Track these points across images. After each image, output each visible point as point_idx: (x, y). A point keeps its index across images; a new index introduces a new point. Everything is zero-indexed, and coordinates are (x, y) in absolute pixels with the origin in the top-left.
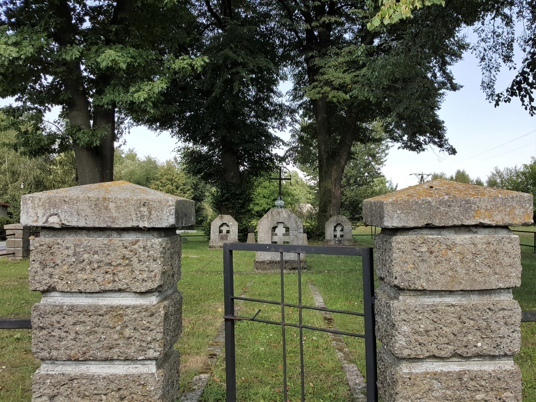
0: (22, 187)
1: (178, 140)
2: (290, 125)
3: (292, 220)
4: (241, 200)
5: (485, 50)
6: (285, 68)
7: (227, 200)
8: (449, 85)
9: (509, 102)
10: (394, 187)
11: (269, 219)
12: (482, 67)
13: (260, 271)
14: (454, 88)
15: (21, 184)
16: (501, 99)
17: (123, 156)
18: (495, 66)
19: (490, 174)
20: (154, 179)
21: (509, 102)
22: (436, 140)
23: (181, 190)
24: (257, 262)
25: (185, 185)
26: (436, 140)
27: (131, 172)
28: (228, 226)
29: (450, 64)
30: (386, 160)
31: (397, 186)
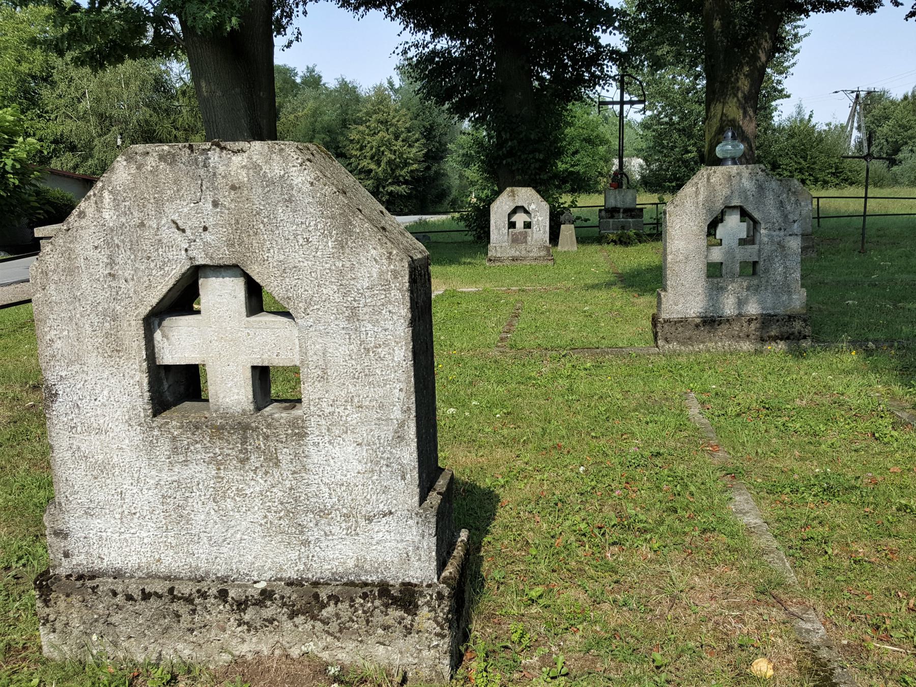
0: (119, 142)
1: (402, 26)
3: (770, 201)
4: (540, 152)
7: (510, 153)
10: (807, 117)
15: (116, 138)
17: (298, 80)
20: (355, 123)
23: (403, 141)
25: (409, 132)
27: (315, 111)
28: (527, 212)
30: (794, 64)
31: (811, 116)
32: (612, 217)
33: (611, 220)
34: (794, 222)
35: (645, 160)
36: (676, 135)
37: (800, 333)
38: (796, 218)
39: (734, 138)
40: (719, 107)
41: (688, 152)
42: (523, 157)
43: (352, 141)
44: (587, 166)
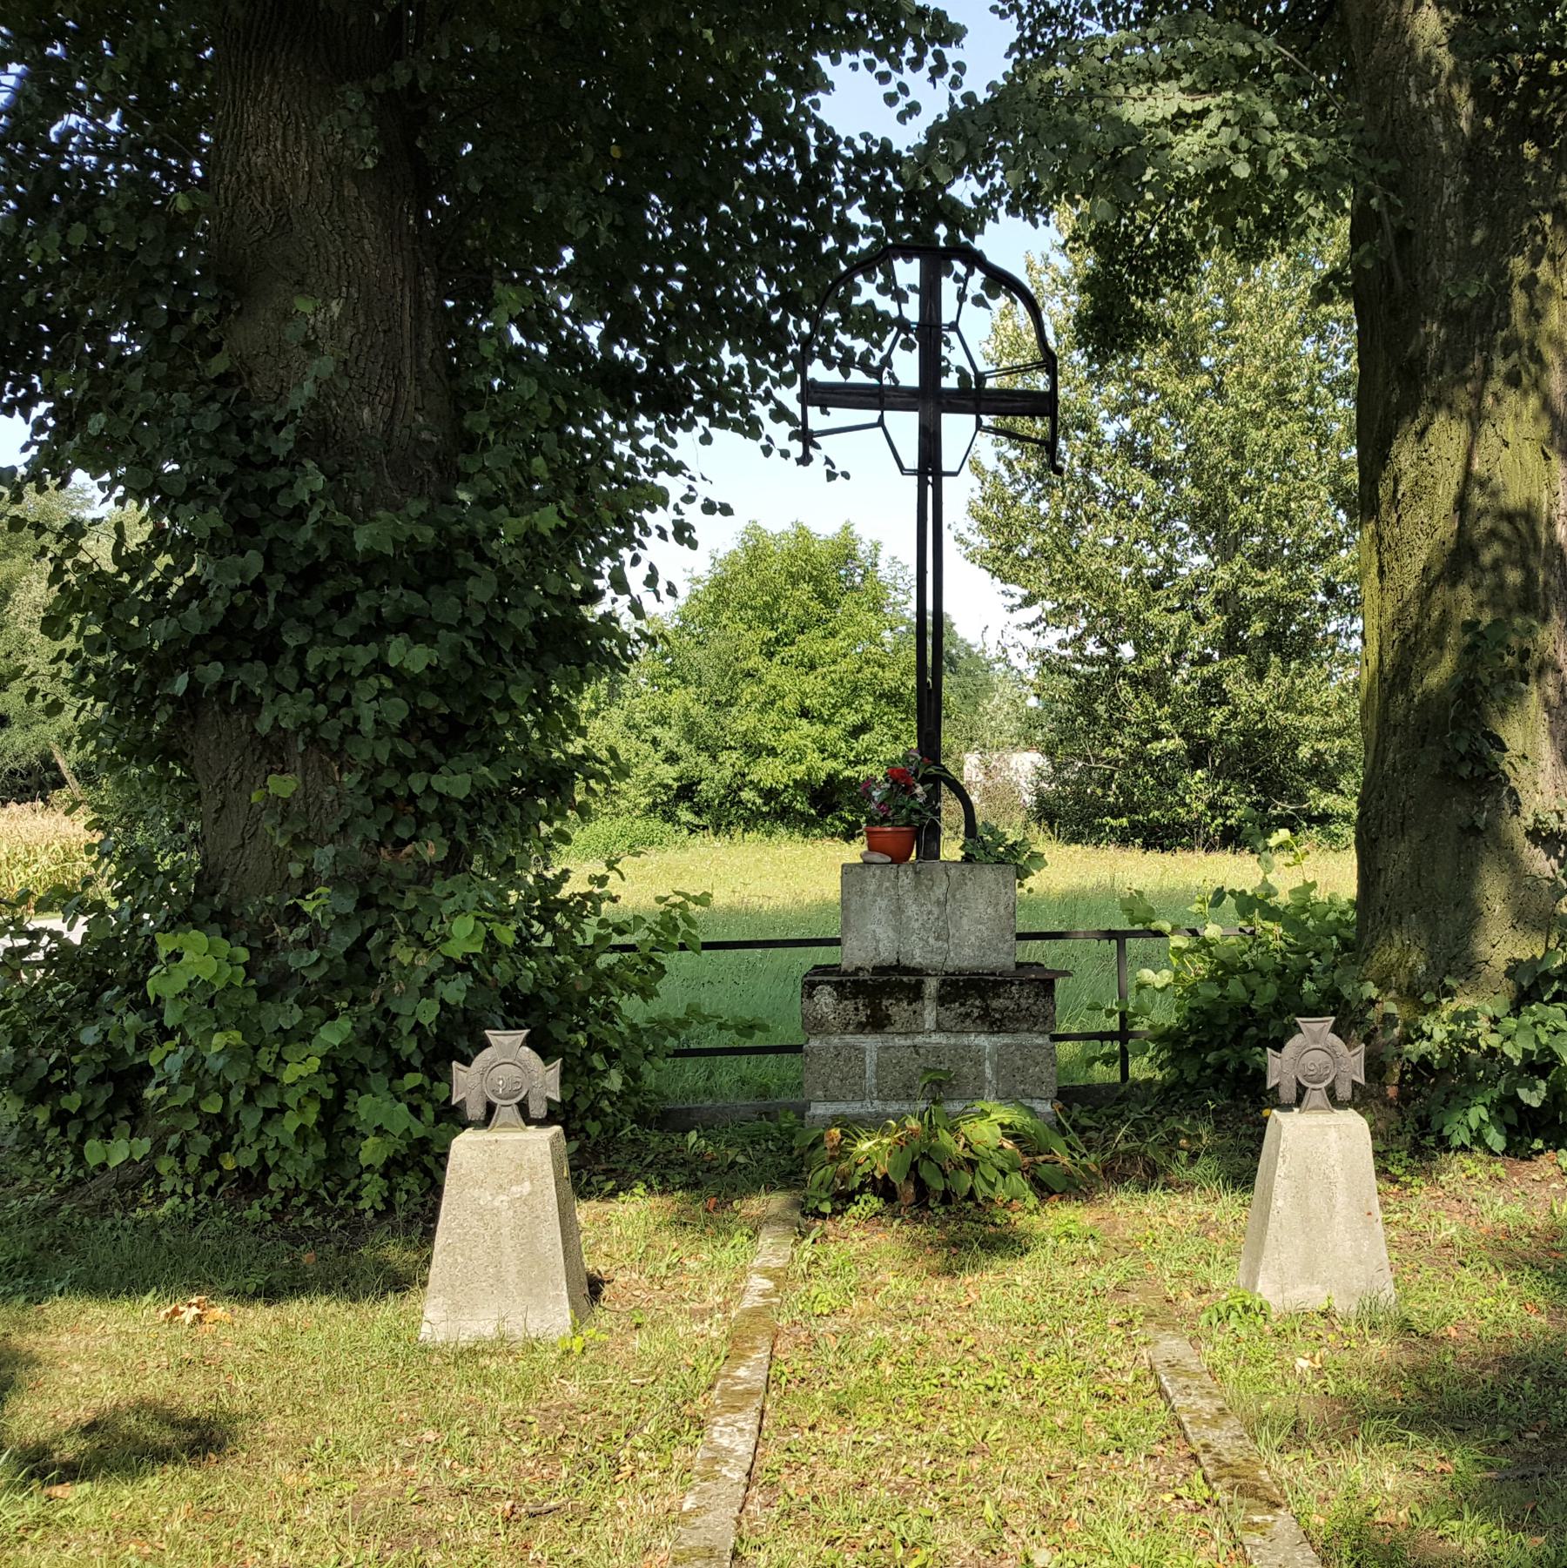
32: (877, 1023)
33: (870, 1043)
35: (1049, 752)
36: (1126, 693)
40: (1447, 436)
41: (1158, 735)
42: (313, 659)
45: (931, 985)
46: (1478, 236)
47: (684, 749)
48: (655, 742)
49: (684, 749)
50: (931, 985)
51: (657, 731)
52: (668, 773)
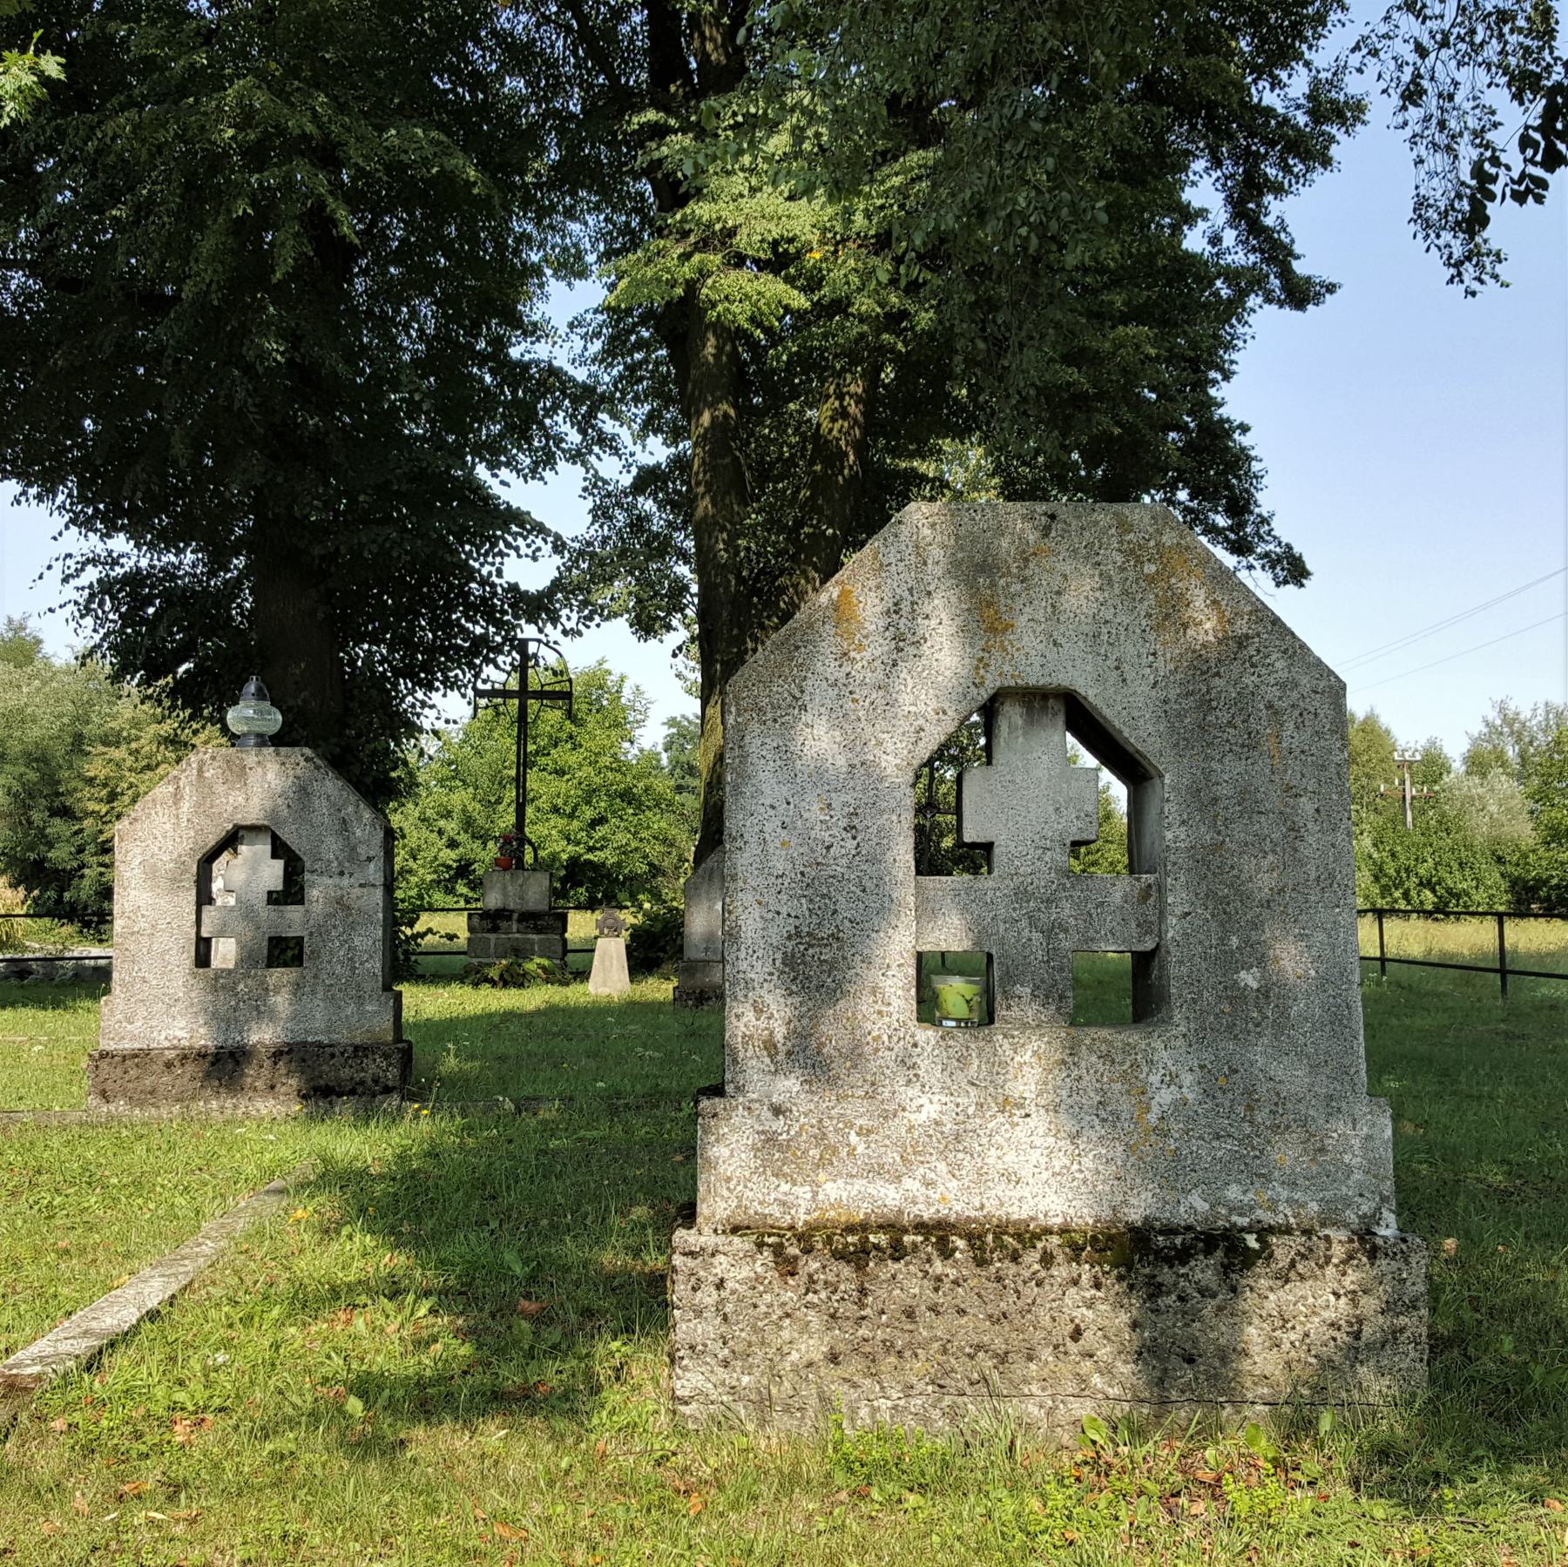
2: (577, 456)
5: (1421, 51)
6: (574, 227)
8: (1275, 283)
9: (1539, 199)
11: (186, 806)
12: (1408, 132)
13: (120, 1106)
14: (1300, 294)
16: (1497, 188)
18: (1472, 123)
19: (1478, 728)
21: (1539, 199)
22: (1221, 521)
24: (104, 1055)
26: (1221, 521)
29: (1278, 190)
32: (495, 929)
33: (492, 936)
34: (369, 859)
37: (376, 1081)
38: (372, 853)
39: (259, 695)
43: (90, 781)
44: (624, 851)
45: (515, 916)
46: (735, 632)
47: (463, 837)
48: (440, 832)
49: (463, 837)
50: (515, 916)
51: (442, 823)
52: (449, 856)
